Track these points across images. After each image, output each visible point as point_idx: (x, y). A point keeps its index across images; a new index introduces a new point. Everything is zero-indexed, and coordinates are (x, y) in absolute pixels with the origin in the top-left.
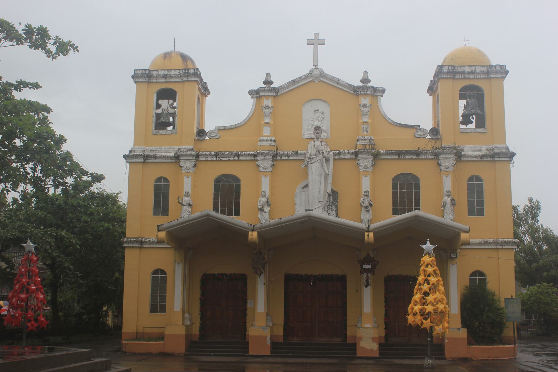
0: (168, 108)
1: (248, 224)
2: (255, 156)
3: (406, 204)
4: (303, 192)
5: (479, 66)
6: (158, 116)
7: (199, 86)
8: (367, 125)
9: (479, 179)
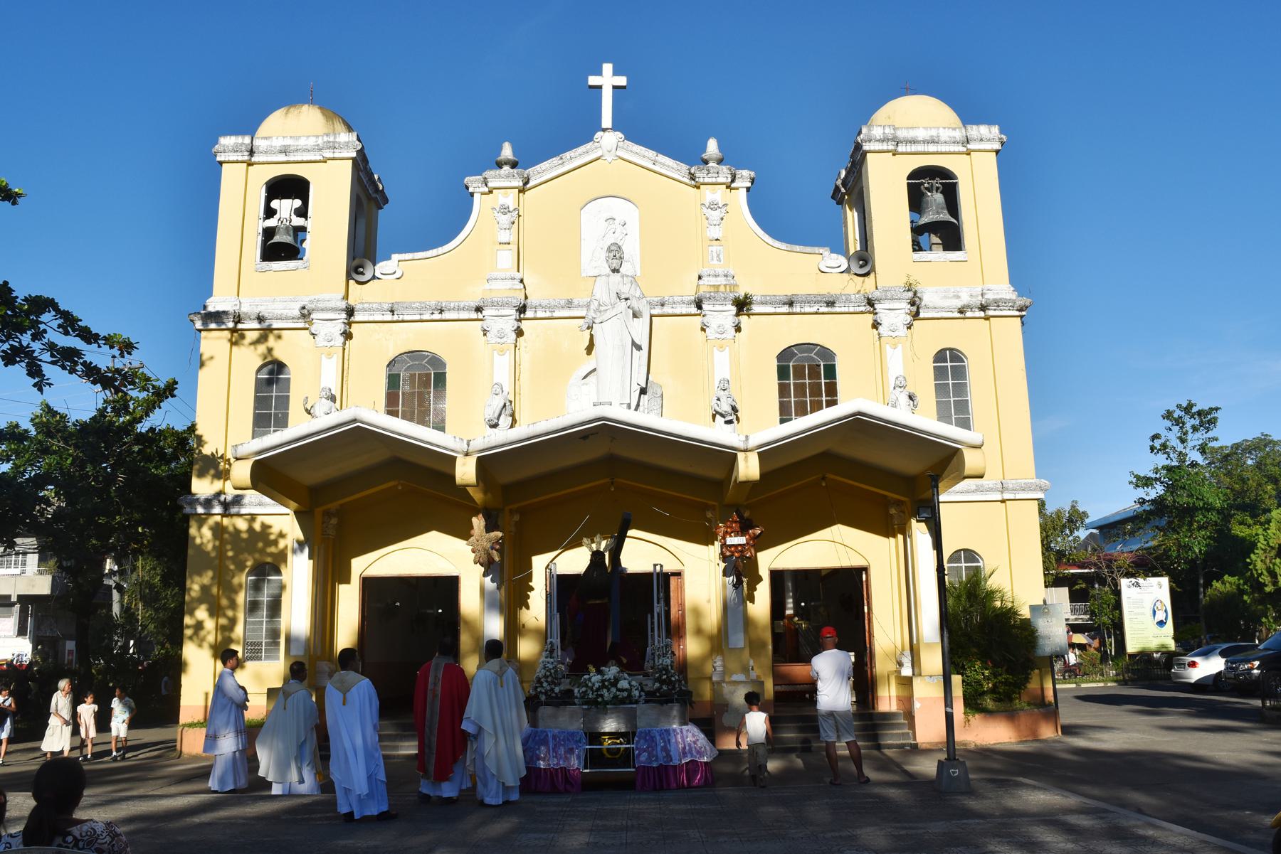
1: (455, 437)
2: (479, 309)
4: (585, 386)
5: (944, 128)
6: (269, 233)
7: (361, 174)
8: (720, 246)
9: (956, 355)
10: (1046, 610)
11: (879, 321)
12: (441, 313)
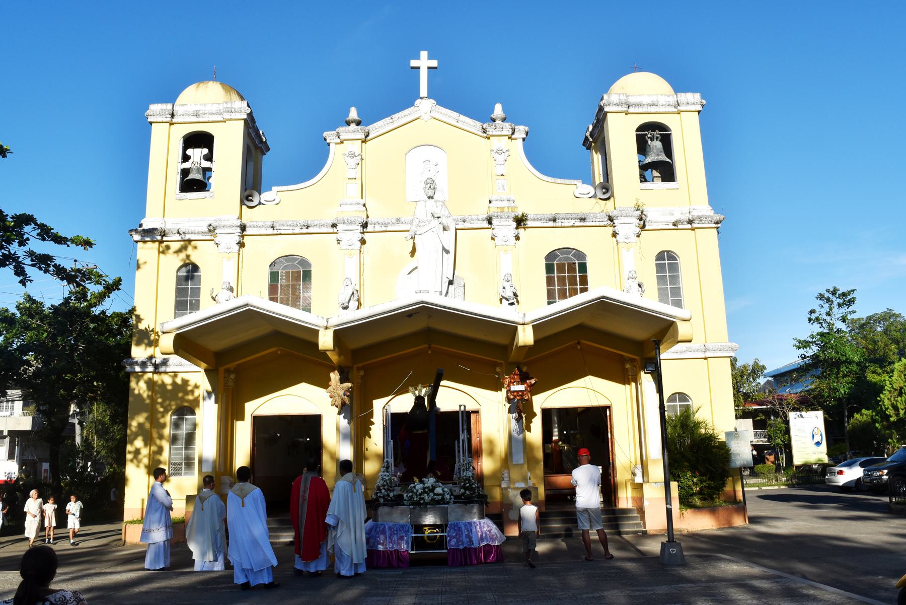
2: (334, 226)
6: (185, 172)
9: (671, 256)
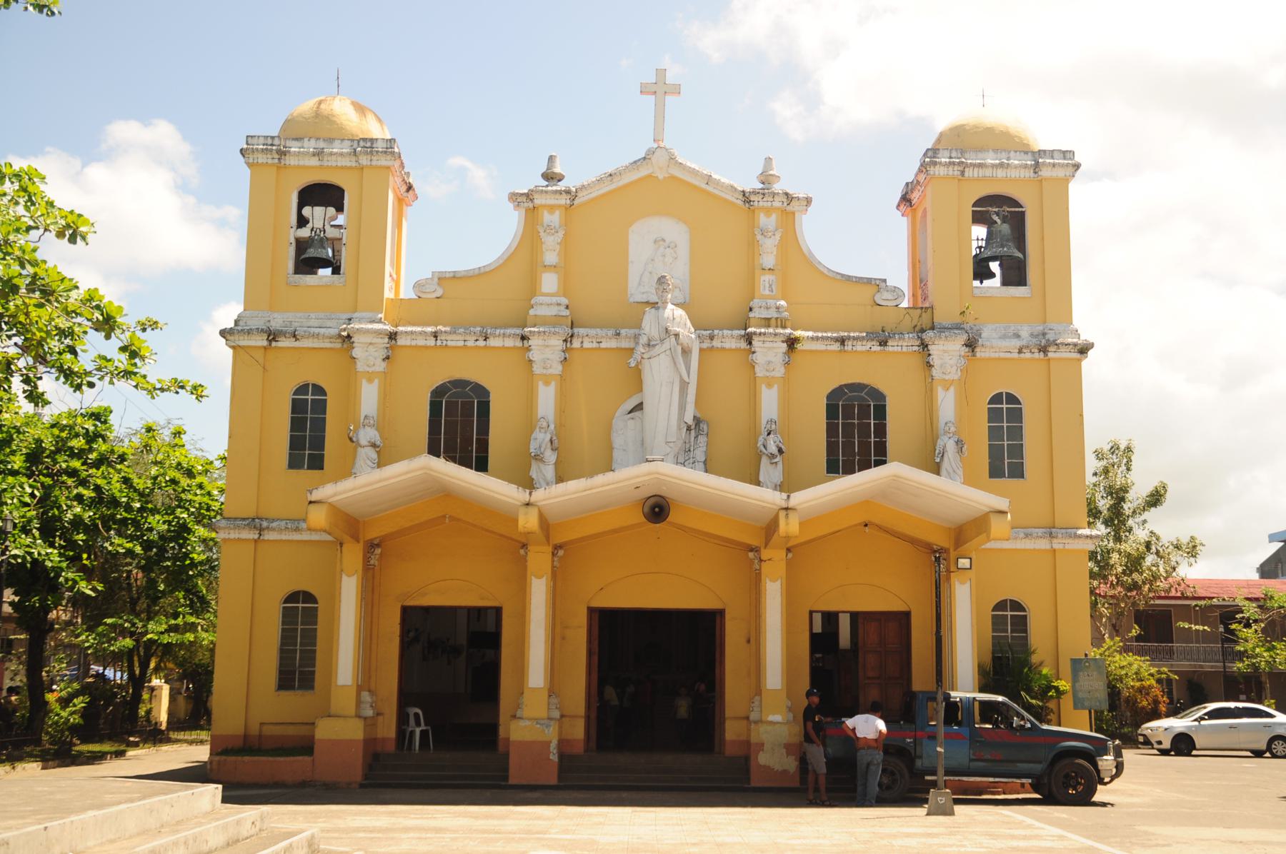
0: (324, 226)
3: (856, 451)
5: (1016, 152)
6: (301, 245)
10: (1087, 664)
11: (932, 363)
12: (485, 340)
